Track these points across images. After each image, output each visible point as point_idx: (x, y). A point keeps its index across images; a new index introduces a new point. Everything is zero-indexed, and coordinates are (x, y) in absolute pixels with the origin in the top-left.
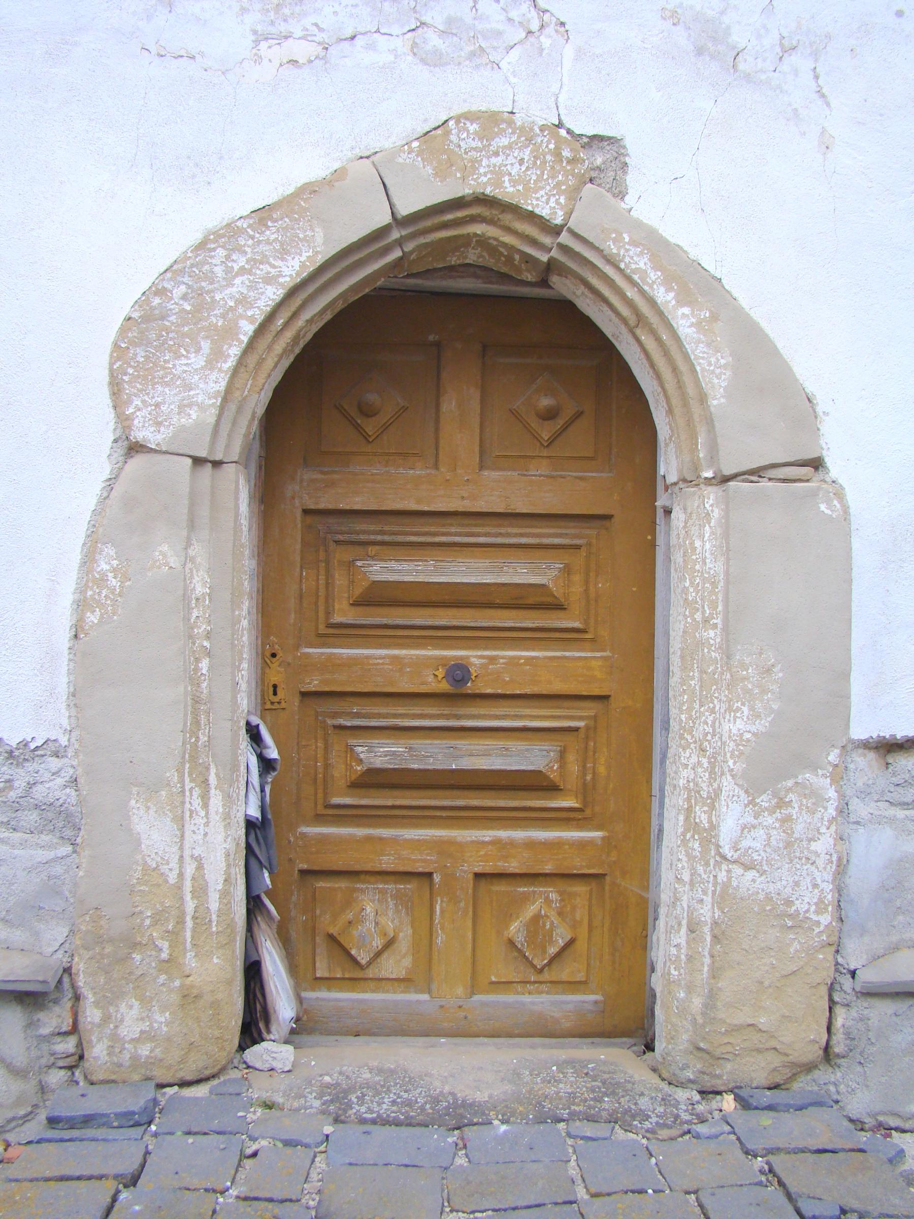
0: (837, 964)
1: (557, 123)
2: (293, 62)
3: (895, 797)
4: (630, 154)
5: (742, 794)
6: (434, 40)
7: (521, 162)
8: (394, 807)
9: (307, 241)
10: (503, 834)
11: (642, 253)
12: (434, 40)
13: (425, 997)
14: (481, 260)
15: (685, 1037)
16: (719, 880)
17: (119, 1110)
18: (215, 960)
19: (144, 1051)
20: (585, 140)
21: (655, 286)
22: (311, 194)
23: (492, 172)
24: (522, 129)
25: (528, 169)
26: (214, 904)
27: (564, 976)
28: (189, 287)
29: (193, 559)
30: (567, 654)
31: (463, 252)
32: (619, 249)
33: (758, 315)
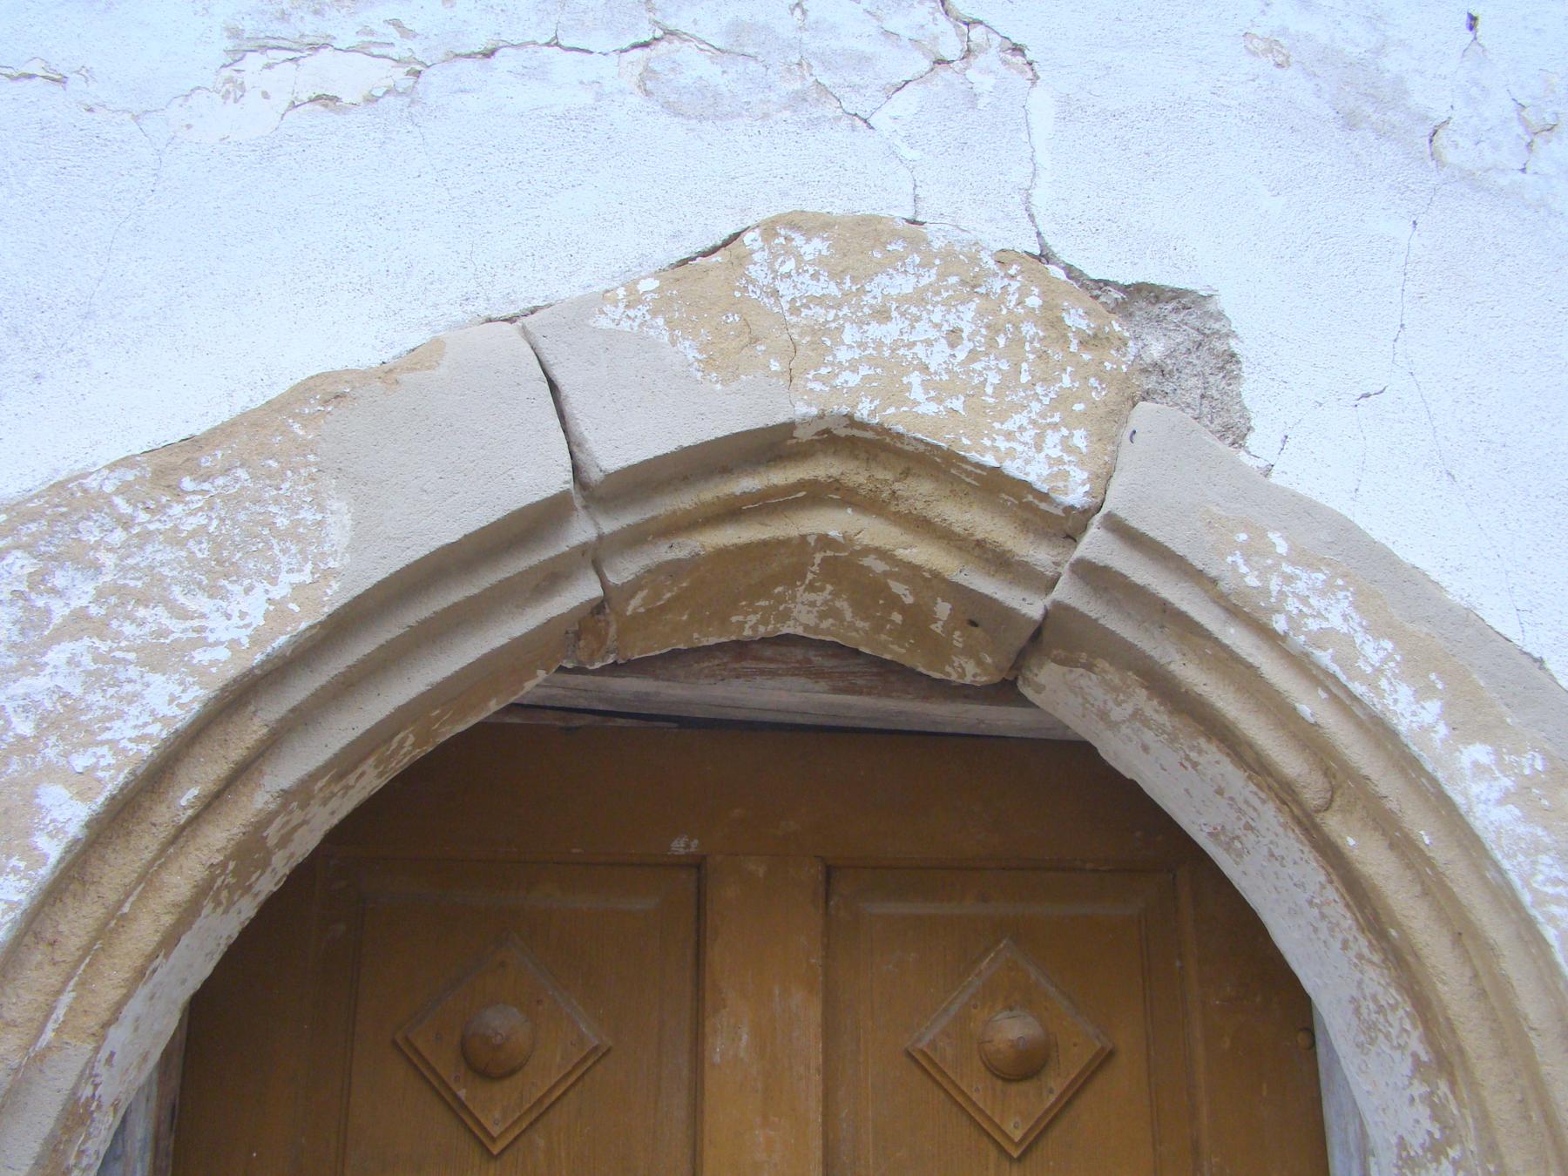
1: (1037, 252)
4: (1239, 332)
6: (696, 66)
7: (954, 336)
9: (299, 539)
12: (696, 66)
14: (826, 624)
21: (1384, 683)
22: (326, 402)
23: (870, 361)
24: (948, 256)
25: (973, 356)
31: (780, 599)
32: (1263, 574)
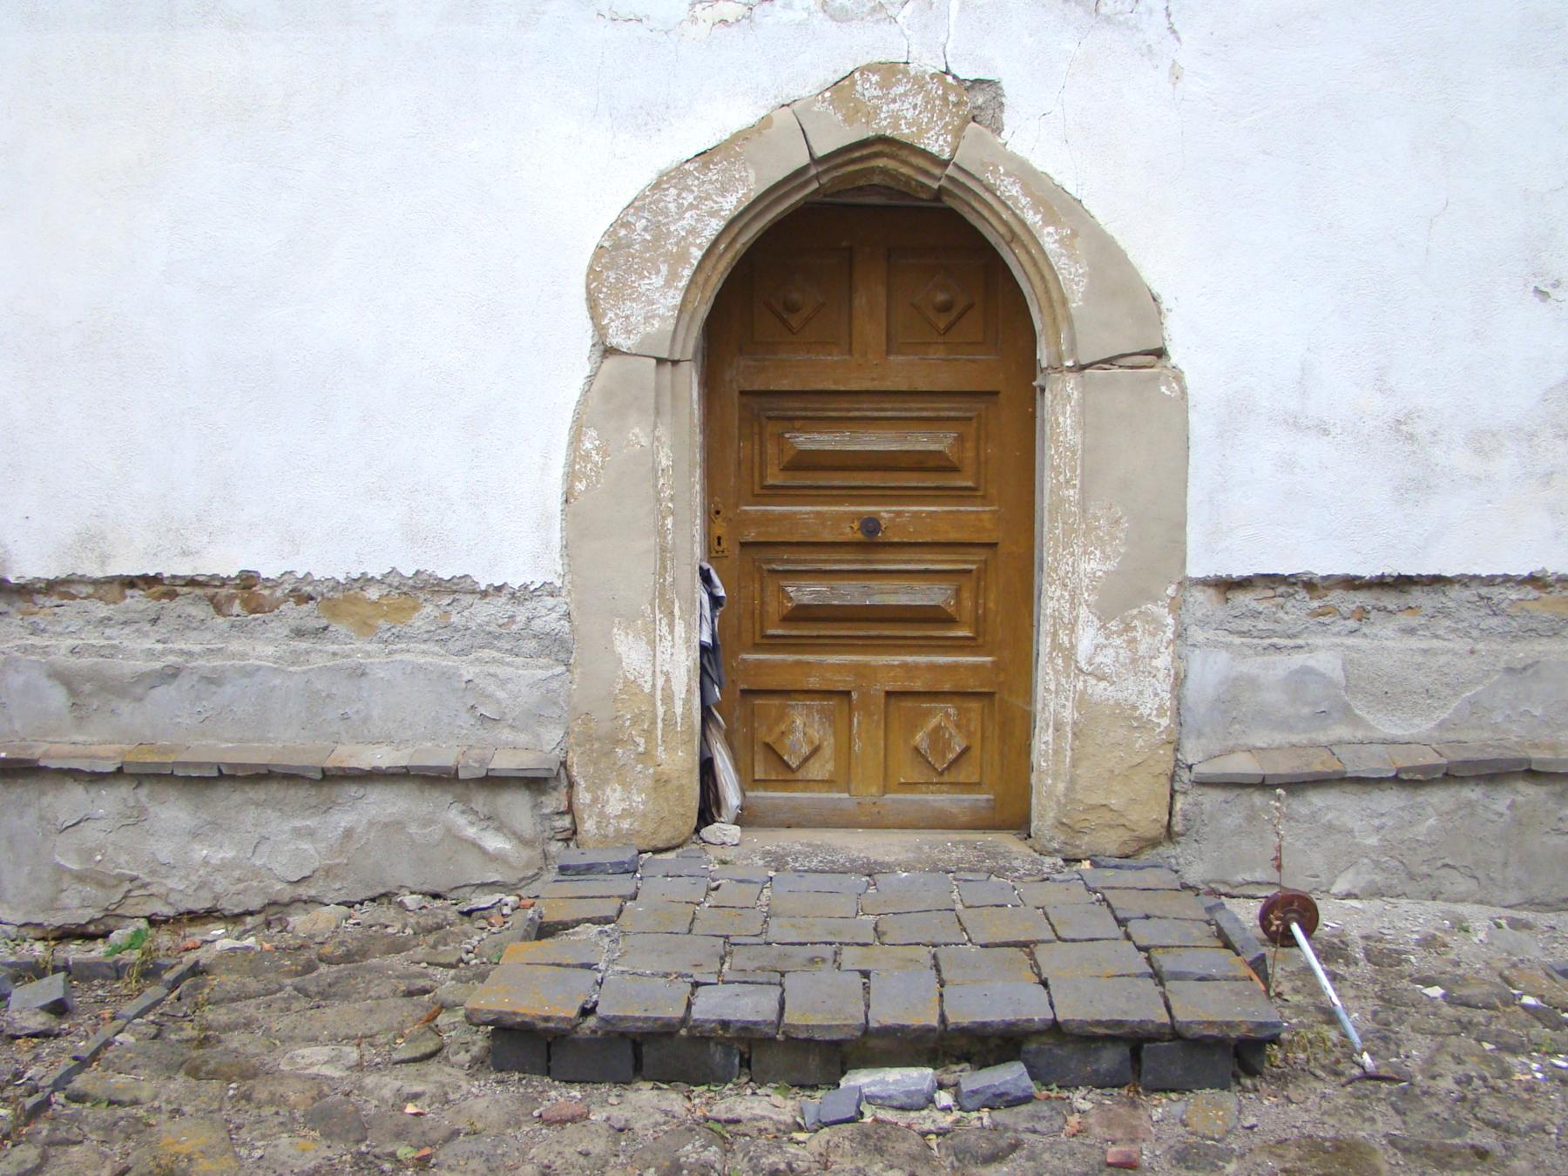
0: (1177, 760)
2: (723, 22)
3: (1234, 626)
5: (1095, 619)
7: (915, 107)
8: (818, 637)
10: (909, 659)
11: (1014, 182)
13: (846, 795)
15: (1051, 815)
16: (1078, 689)
17: (612, 861)
18: (680, 754)
19: (625, 825)
20: (968, 84)
24: (915, 77)
25: (920, 112)
26: (679, 710)
27: (961, 779)
28: (648, 220)
29: (658, 439)
30: (961, 508)
33: (1111, 230)
